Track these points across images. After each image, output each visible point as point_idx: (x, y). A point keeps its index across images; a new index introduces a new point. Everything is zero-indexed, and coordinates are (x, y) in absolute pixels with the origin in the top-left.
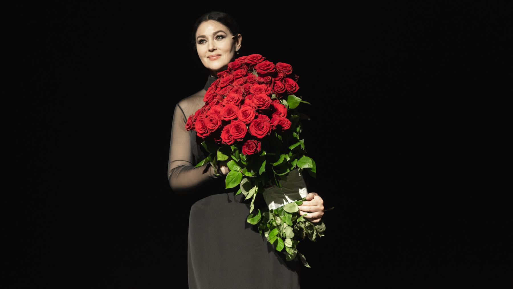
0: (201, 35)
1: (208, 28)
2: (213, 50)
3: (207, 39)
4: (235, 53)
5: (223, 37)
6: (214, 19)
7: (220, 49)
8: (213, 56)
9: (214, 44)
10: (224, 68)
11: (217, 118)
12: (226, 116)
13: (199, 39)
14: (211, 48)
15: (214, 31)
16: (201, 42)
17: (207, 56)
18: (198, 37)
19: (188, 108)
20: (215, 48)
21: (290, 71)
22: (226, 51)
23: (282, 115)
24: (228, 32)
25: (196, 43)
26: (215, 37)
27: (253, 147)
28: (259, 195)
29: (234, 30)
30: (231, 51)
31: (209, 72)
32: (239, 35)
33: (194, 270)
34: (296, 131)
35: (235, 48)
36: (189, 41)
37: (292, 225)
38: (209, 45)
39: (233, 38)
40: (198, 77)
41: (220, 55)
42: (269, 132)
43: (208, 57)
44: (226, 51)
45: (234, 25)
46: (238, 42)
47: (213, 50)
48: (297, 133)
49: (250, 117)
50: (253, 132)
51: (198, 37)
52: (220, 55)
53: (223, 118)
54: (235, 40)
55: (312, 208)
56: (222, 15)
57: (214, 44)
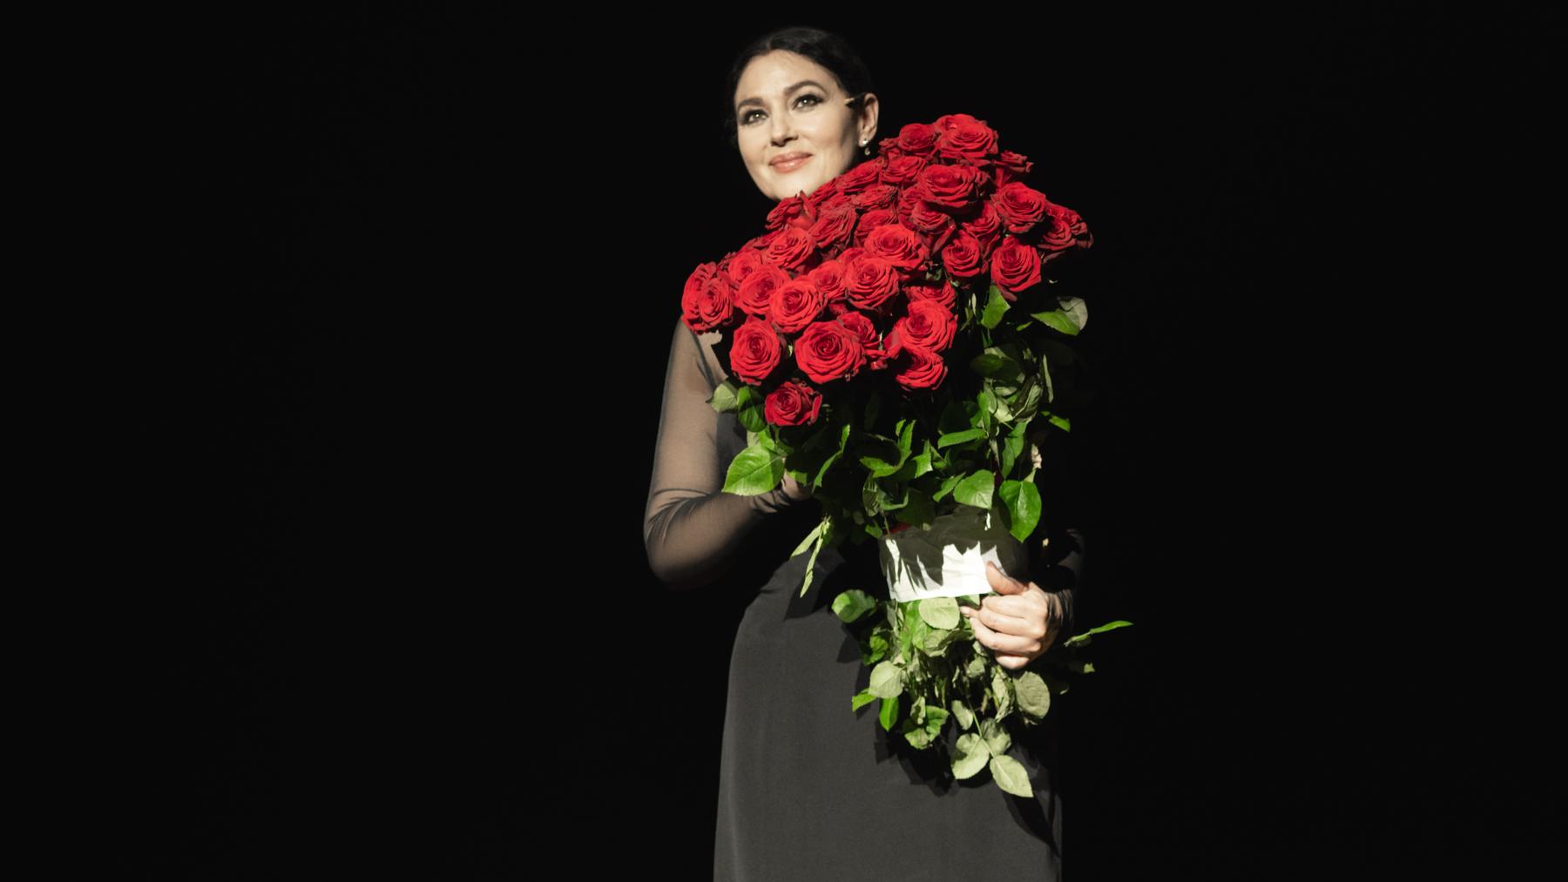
0: (750, 95)
1: (771, 76)
5: (812, 100)
6: (791, 48)
7: (806, 137)
8: (785, 160)
9: (792, 125)
10: (824, 194)
11: (725, 295)
12: (750, 302)
13: (743, 111)
14: (778, 134)
15: (789, 84)
18: (742, 105)
20: (791, 134)
21: (1024, 223)
22: (827, 143)
23: (928, 341)
26: (792, 99)
27: (793, 409)
28: (997, 499)
29: (852, 81)
32: (868, 96)
33: (731, 672)
35: (857, 137)
36: (718, 116)
37: (891, 613)
38: (772, 125)
39: (849, 105)
41: (809, 155)
42: (850, 370)
43: (771, 164)
44: (827, 143)
46: (865, 117)
47: (787, 140)
49: (802, 314)
50: (804, 355)
51: (742, 105)
52: (809, 155)
53: (739, 304)
54: (857, 110)
55: (1002, 621)
56: (816, 35)
57: (792, 125)
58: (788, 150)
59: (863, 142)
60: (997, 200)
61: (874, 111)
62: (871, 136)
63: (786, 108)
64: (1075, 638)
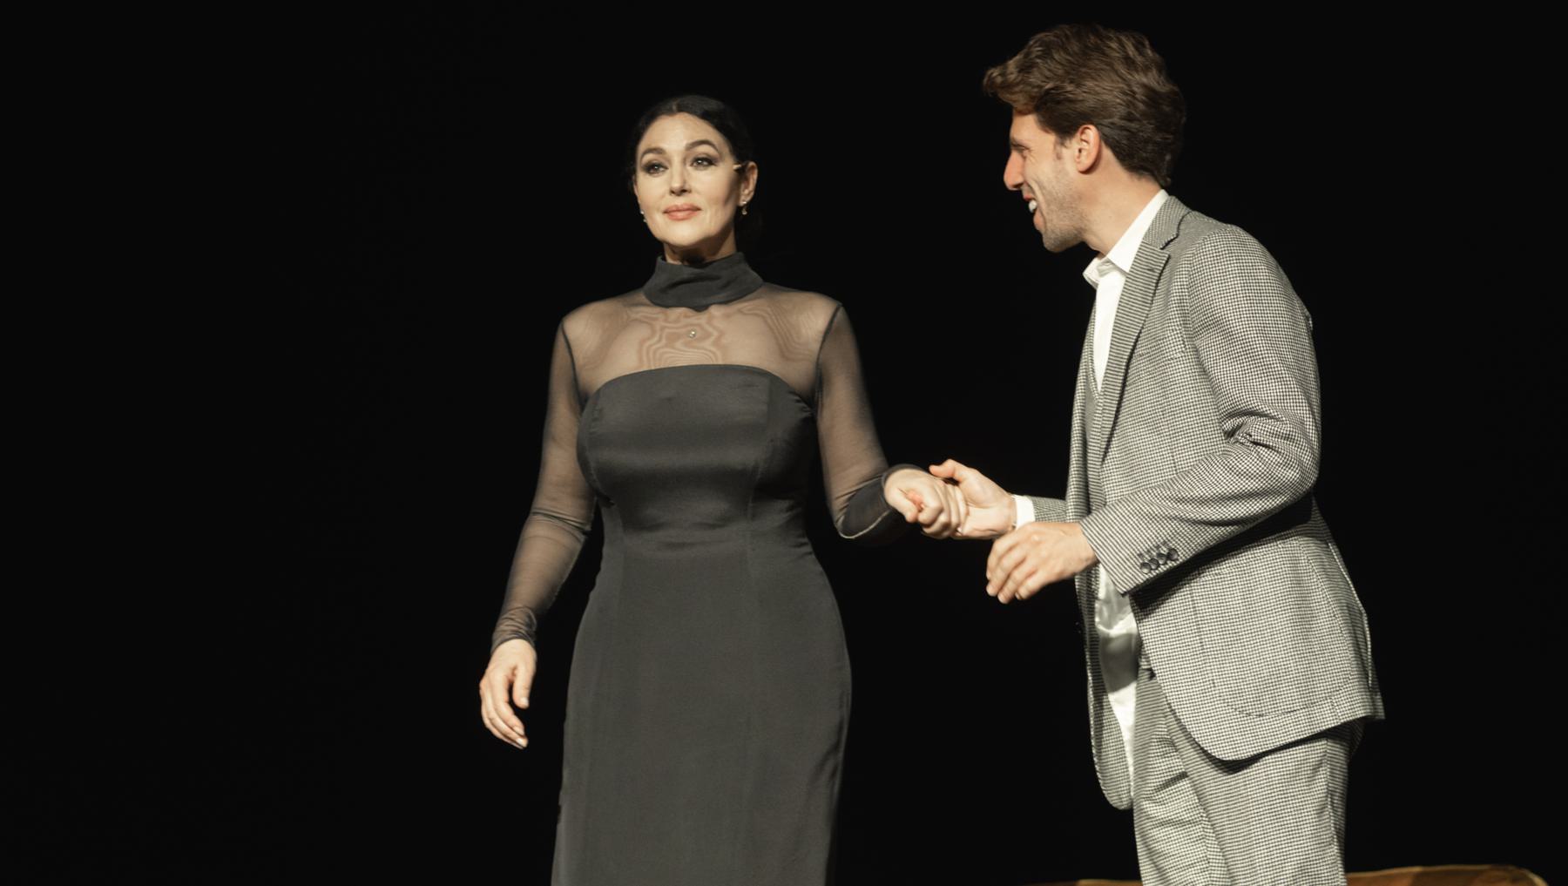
1: (674, 134)
2: (683, 191)
3: (669, 161)
4: (739, 209)
5: (709, 161)
9: (685, 179)
13: (649, 157)
14: (676, 185)
16: (652, 168)
17: (663, 208)
18: (650, 151)
19: (614, 344)
24: (726, 150)
25: (634, 172)
29: (740, 154)
30: (726, 201)
31: (657, 246)
33: (562, 828)
34: (626, 261)
36: (618, 162)
38: (672, 177)
40: (626, 261)
43: (666, 212)
45: (745, 136)
46: (747, 180)
47: (683, 191)
48: (699, 278)
51: (650, 151)
54: (741, 176)
56: (713, 105)
57: (685, 179)
58: (680, 201)
59: (743, 202)
60: (1201, 605)
61: (753, 178)
62: (972, 478)
63: (684, 161)
64: (752, 186)
